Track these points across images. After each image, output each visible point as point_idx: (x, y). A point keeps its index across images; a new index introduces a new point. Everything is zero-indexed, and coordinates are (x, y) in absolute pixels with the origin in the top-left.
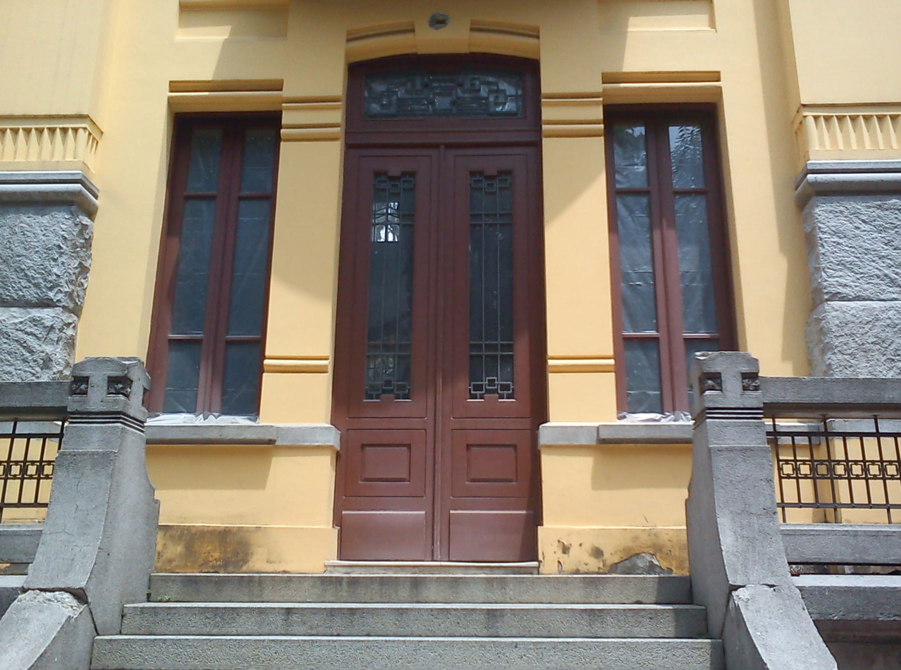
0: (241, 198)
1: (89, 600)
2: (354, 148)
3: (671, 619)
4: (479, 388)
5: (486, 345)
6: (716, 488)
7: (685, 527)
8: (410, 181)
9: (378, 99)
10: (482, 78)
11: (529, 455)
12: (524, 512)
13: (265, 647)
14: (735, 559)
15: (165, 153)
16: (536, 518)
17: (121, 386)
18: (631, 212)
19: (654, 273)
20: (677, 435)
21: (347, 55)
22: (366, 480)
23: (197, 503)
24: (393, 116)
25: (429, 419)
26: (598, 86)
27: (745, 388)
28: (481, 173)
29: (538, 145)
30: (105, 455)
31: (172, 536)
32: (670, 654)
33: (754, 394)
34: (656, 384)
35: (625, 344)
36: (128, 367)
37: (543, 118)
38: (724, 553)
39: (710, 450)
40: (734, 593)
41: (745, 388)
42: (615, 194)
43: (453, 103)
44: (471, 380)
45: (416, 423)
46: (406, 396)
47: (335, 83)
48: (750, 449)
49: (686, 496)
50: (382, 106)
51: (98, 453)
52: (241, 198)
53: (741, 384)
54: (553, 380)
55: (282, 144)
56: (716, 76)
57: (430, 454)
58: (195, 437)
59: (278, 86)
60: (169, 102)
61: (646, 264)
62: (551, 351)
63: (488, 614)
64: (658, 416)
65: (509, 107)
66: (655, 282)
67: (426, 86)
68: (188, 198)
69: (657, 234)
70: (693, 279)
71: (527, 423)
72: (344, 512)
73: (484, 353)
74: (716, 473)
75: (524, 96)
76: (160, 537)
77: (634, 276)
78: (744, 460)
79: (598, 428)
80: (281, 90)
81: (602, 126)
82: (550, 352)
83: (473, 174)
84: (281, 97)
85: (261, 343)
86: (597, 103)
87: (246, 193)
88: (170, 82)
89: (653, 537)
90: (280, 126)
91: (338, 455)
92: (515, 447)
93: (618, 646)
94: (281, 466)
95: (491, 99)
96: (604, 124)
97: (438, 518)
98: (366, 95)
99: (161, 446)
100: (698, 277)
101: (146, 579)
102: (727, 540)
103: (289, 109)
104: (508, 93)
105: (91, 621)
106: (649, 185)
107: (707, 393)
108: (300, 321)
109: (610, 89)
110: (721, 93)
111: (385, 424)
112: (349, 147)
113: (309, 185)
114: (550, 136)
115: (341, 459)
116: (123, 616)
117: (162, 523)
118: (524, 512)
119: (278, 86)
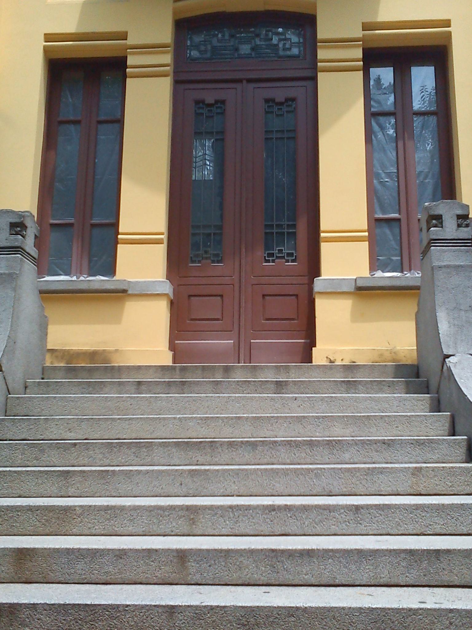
0: (100, 122)
1: (3, 369)
2: (180, 83)
3: (403, 387)
4: (272, 255)
5: (276, 233)
6: (436, 293)
7: (416, 348)
8: (221, 107)
9: (197, 47)
10: (274, 30)
11: (306, 302)
12: (303, 341)
13: (123, 401)
14: (448, 339)
15: (43, 90)
16: (312, 343)
17: (19, 229)
18: (382, 128)
19: (398, 172)
20: (411, 283)
21: (175, 13)
22: (192, 320)
23: (72, 333)
24: (209, 59)
25: (236, 277)
26: (359, 33)
27: (459, 226)
28: (273, 100)
29: (314, 79)
30: (10, 275)
31: (57, 357)
32: (401, 404)
33: (465, 229)
34: (398, 252)
35: (375, 223)
36: (24, 217)
37: (319, 57)
38: (440, 335)
39: (432, 268)
40: (447, 360)
41: (459, 226)
42: (372, 115)
43: (253, 49)
44: (265, 250)
45: (227, 280)
46: (218, 262)
47: (165, 34)
48: (462, 266)
49: (416, 310)
50: (200, 52)
51: (5, 274)
52: (100, 122)
53: (456, 223)
54: (324, 247)
55: (128, 79)
56: (447, 23)
57: (236, 308)
58: (71, 288)
59: (124, 36)
60: (44, 50)
61: (392, 166)
62: (323, 226)
63: (276, 384)
64: (399, 274)
65: (295, 51)
66: (398, 179)
67: (232, 36)
68: (61, 123)
69: (400, 144)
70: (426, 177)
71: (305, 280)
72: (176, 342)
73: (275, 231)
74: (437, 283)
75: (304, 43)
76: (48, 357)
77: (383, 175)
78: (457, 274)
79: (356, 280)
80: (126, 40)
81: (362, 63)
82: (322, 227)
83: (267, 101)
84: (126, 44)
85: (115, 225)
86: (358, 46)
87: (102, 118)
88: (45, 34)
89: (393, 354)
90: (126, 67)
91: (172, 303)
92: (297, 296)
93: (366, 399)
94: (133, 309)
95: (281, 45)
96: (363, 61)
97: (242, 345)
98: (189, 43)
99: (47, 294)
100: (430, 175)
101: (40, 368)
102: (444, 327)
103: (132, 53)
104: (293, 41)
105: (5, 384)
106: (395, 108)
107: (432, 229)
108: (143, 207)
109: (369, 35)
110: (451, 35)
111: (204, 281)
112: (177, 82)
113: (148, 111)
114: (328, 240)
115: (175, 306)
116: (26, 387)
117: (49, 348)
118: (303, 341)
119: (124, 36)
